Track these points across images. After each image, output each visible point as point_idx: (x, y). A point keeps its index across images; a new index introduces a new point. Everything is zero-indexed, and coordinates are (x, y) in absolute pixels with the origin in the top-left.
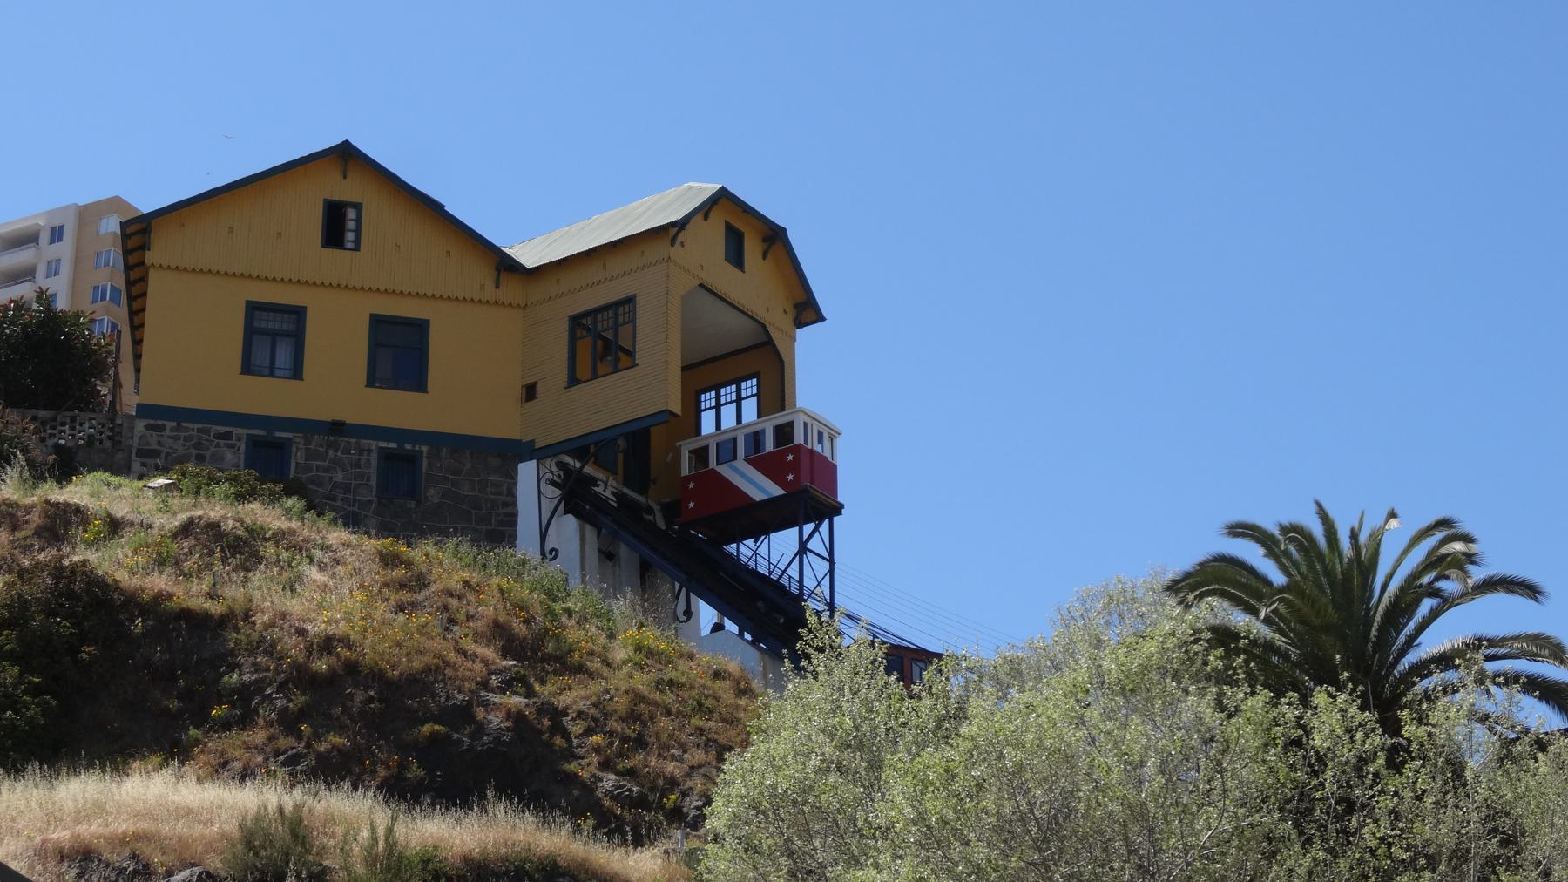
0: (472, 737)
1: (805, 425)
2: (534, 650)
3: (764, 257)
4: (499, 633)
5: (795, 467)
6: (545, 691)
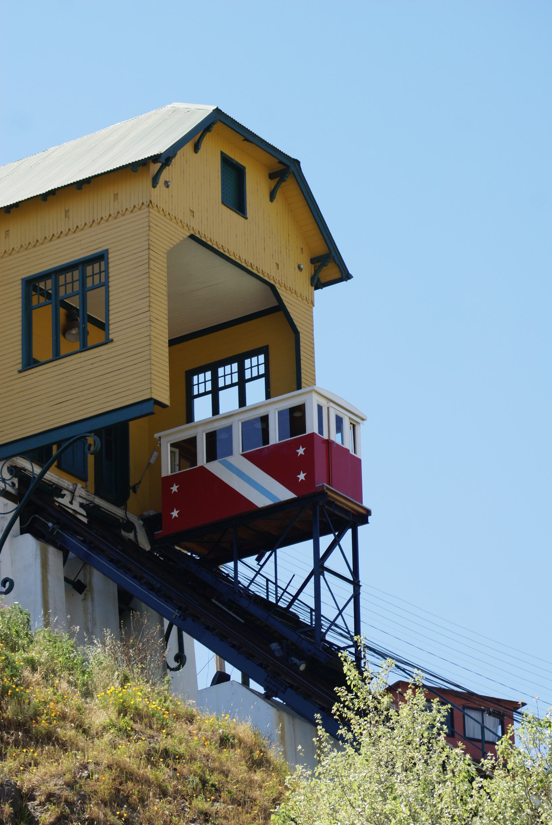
1: (320, 408)
3: (272, 197)
5: (307, 463)
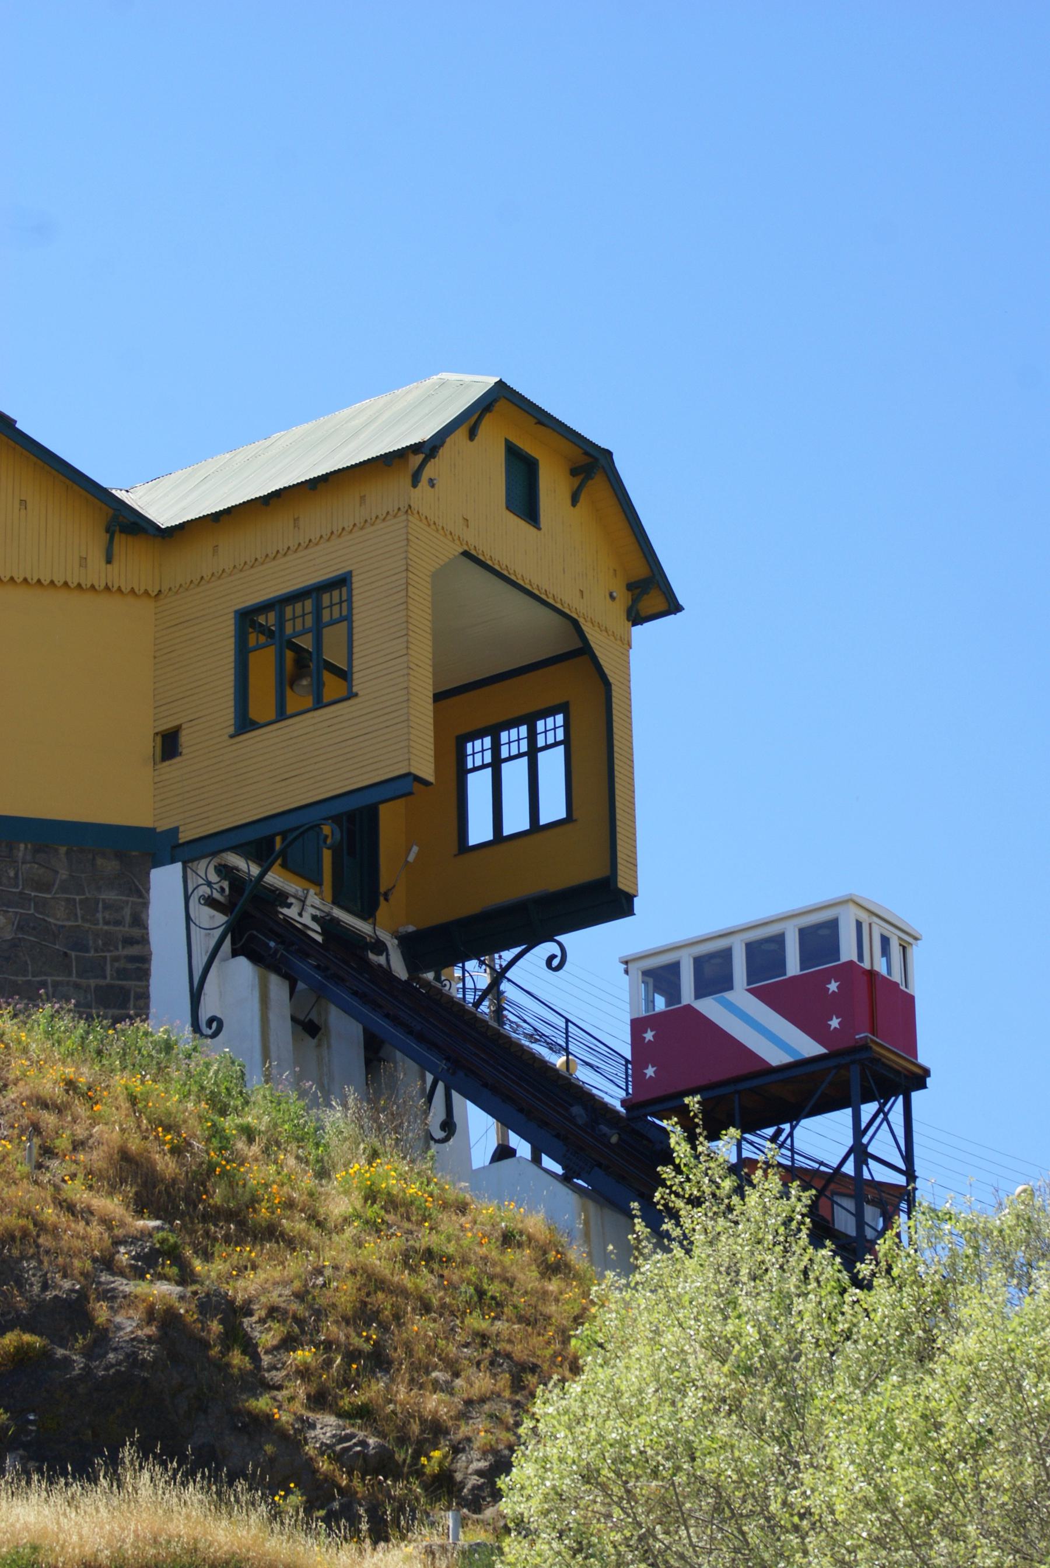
0: (89, 1353)
1: (859, 925)
2: (188, 1201)
3: (575, 500)
4: (130, 1171)
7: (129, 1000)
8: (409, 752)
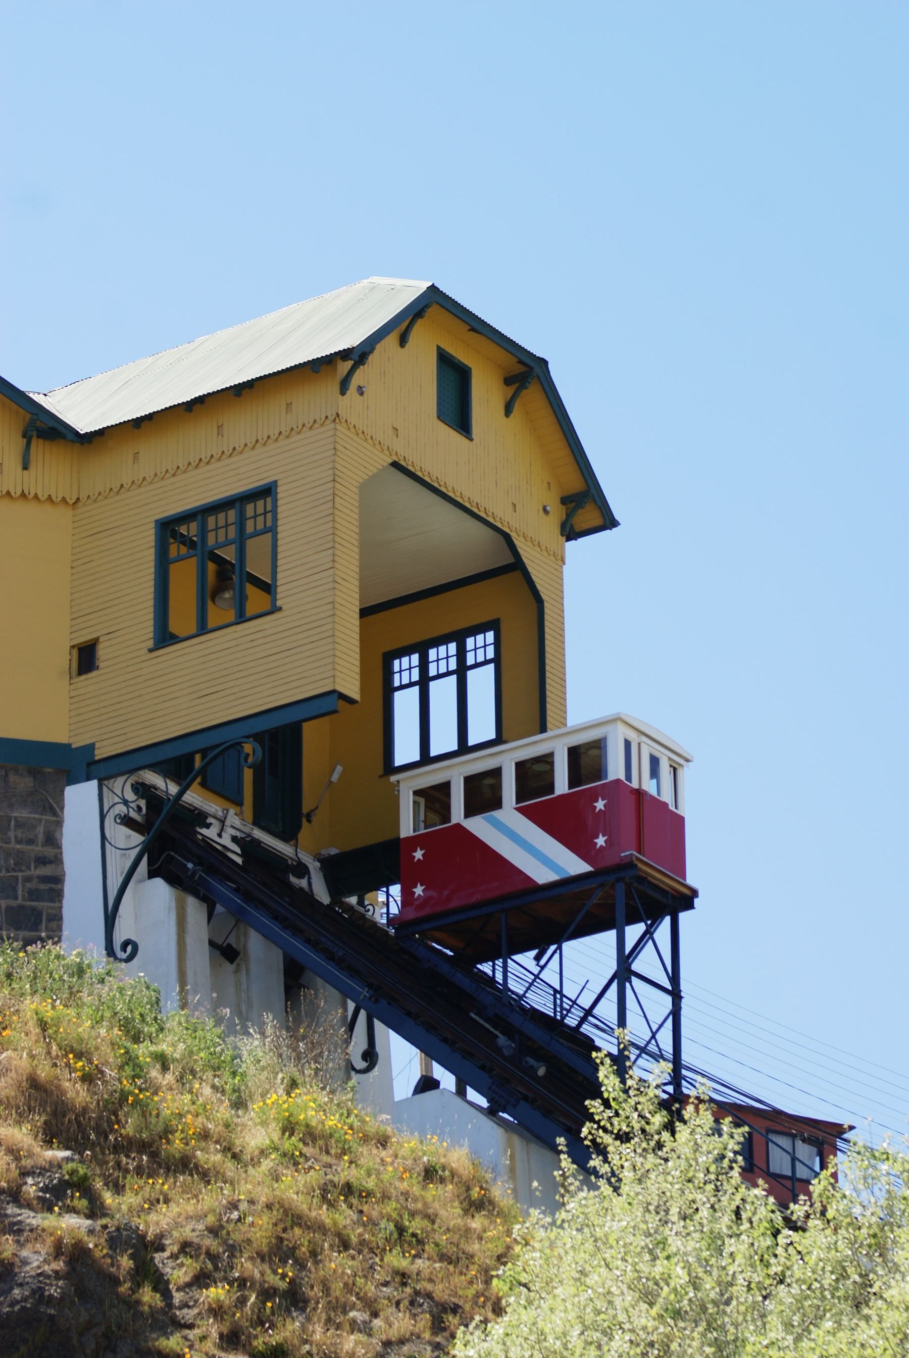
1: (628, 744)
3: (508, 410)
6: (121, 1204)
7: (41, 921)
8: (334, 669)
